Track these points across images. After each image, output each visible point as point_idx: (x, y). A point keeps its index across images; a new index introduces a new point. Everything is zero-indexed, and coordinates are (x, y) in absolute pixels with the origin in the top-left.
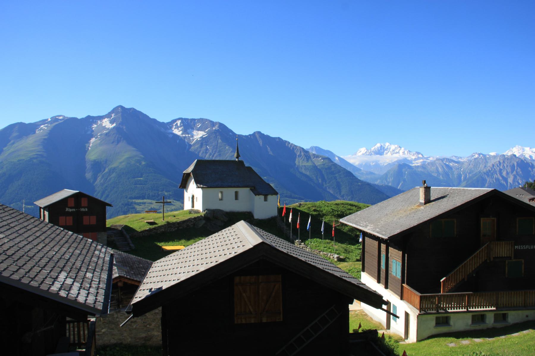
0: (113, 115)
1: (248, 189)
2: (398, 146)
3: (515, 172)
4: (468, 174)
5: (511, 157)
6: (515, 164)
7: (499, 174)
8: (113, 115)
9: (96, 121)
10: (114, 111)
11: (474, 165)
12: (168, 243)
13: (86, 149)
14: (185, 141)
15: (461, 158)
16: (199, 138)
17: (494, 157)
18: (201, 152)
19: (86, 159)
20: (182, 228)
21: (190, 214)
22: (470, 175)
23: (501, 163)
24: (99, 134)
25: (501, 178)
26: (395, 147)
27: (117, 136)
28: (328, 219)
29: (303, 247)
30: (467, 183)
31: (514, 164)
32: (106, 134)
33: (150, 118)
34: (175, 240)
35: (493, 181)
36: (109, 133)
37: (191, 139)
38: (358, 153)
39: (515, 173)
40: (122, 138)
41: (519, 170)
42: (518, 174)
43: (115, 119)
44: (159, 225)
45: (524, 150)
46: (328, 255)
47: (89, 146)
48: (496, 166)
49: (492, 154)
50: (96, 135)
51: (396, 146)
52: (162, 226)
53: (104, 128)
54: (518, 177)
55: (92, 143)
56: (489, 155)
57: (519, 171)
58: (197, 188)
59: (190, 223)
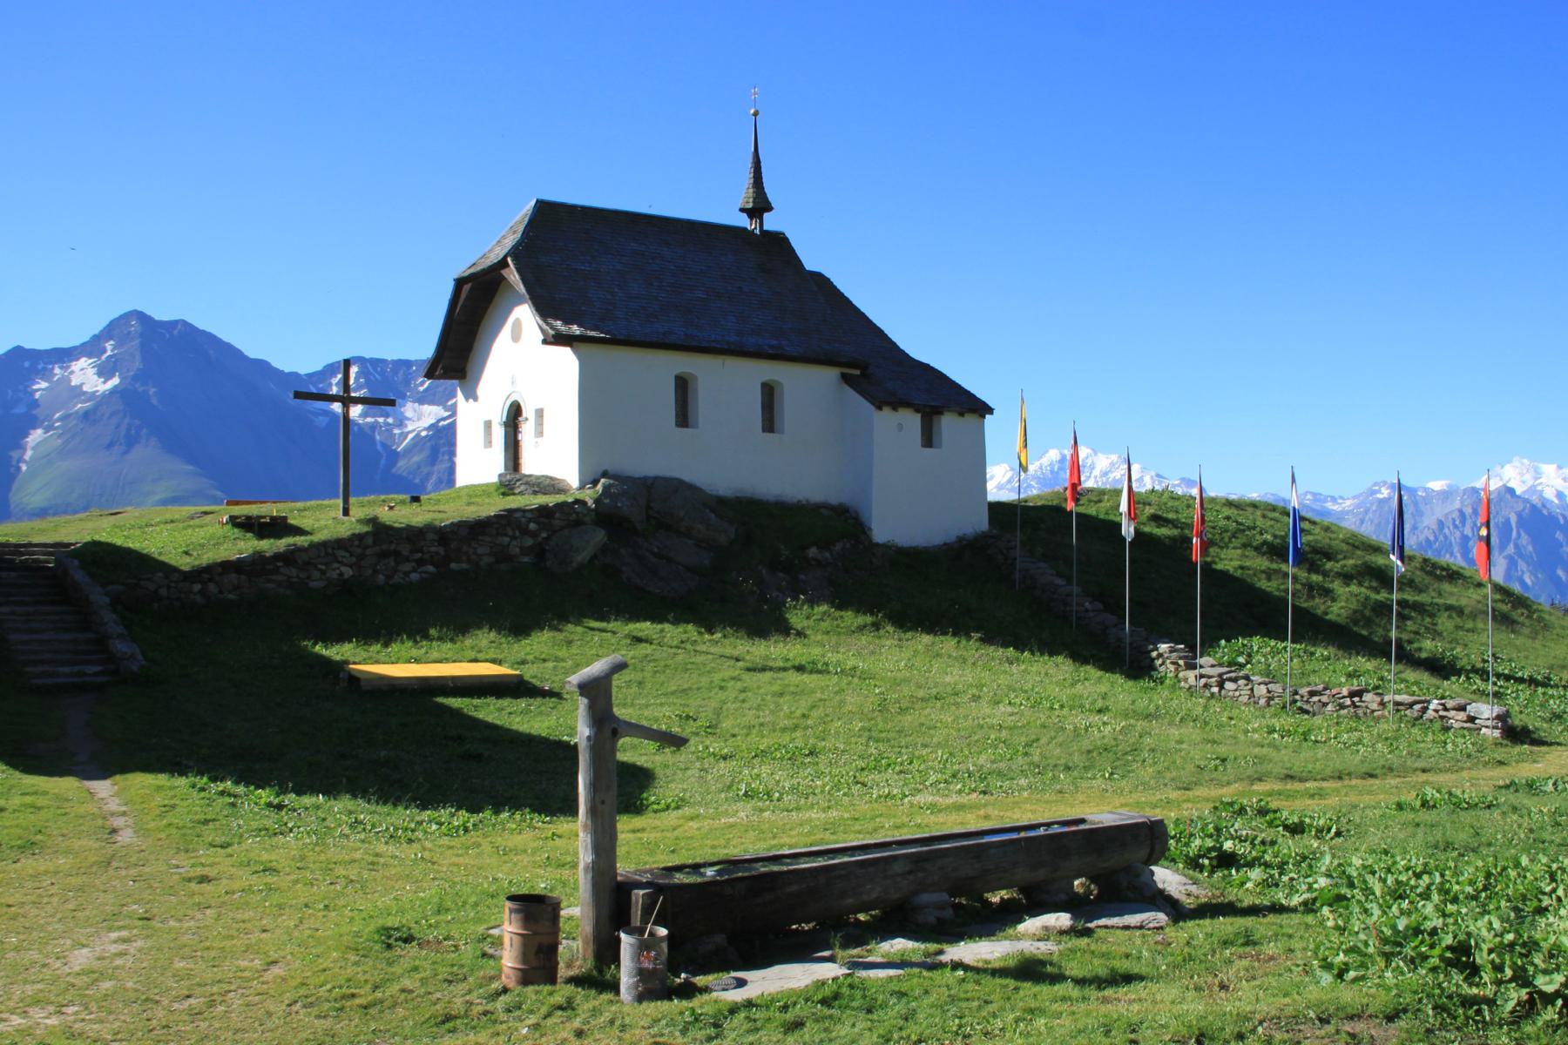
0: (109, 346)
1: (832, 374)
2: (1120, 457)
3: (1512, 545)
5: (1499, 494)
6: (1513, 519)
7: (1459, 555)
8: (109, 346)
9: (45, 369)
10: (114, 329)
11: (1379, 525)
12: (386, 645)
13: (12, 470)
14: (373, 438)
15: (1334, 499)
16: (425, 429)
17: (1446, 495)
18: (434, 479)
19: (12, 507)
20: (464, 566)
21: (504, 494)
23: (1468, 517)
24: (57, 415)
26: (1110, 461)
27: (127, 421)
28: (1236, 563)
29: (1220, 675)
31: (1507, 522)
32: (86, 415)
33: (246, 358)
34: (433, 632)
36: (95, 409)
37: (397, 431)
39: (1511, 549)
40: (145, 430)
41: (1525, 539)
42: (1521, 556)
43: (115, 363)
44: (318, 538)
45: (1538, 474)
46: (1425, 710)
47: (20, 460)
48: (1451, 527)
49: (1437, 485)
50: (49, 417)
51: (1114, 457)
52: (339, 544)
53: (78, 392)
54: (1522, 565)
55: (33, 448)
56: (1426, 489)
57: (1524, 542)
58: (545, 342)
59: (514, 538)
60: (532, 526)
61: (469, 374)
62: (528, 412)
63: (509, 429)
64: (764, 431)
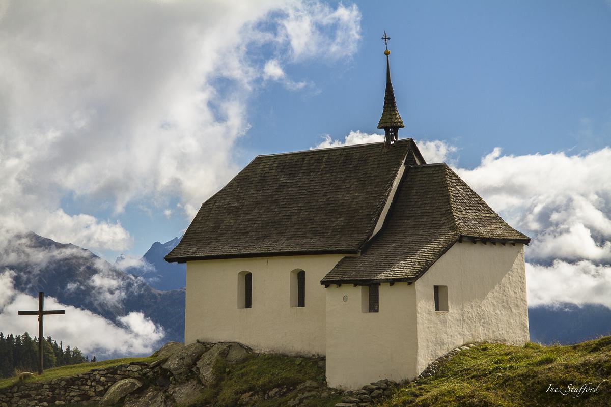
20: (62, 403)
61: (393, 286)
64: (251, 308)
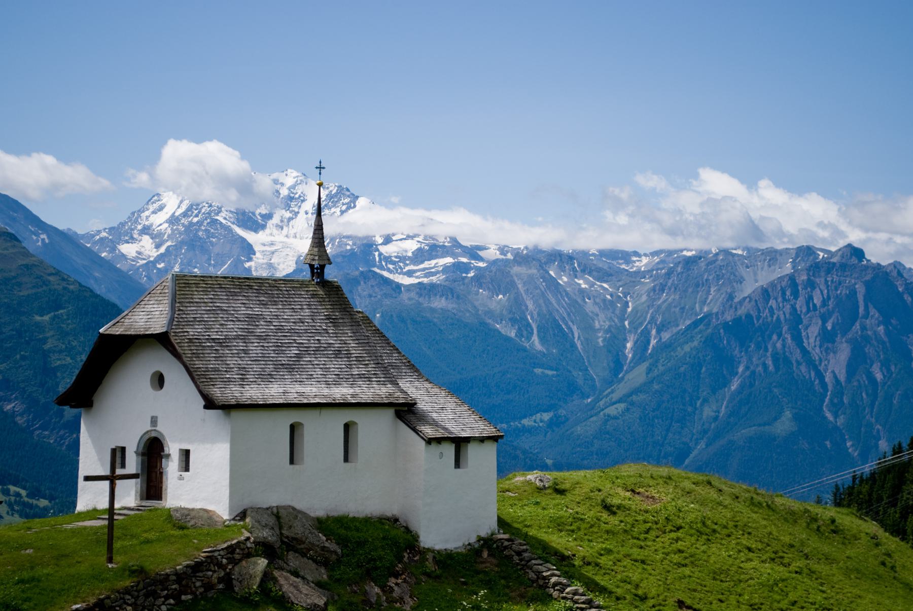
4: (654, 332)
7: (788, 336)
22: (666, 336)
25: (797, 355)
30: (649, 370)
35: (765, 366)
38: (147, 213)
59: (214, 571)
60: (224, 561)
61: (96, 405)
62: (173, 448)
63: (144, 458)
